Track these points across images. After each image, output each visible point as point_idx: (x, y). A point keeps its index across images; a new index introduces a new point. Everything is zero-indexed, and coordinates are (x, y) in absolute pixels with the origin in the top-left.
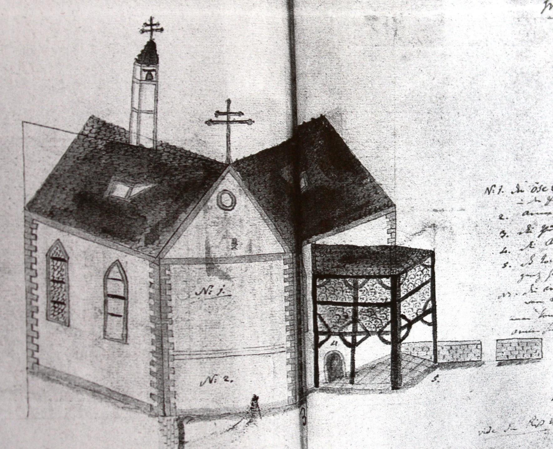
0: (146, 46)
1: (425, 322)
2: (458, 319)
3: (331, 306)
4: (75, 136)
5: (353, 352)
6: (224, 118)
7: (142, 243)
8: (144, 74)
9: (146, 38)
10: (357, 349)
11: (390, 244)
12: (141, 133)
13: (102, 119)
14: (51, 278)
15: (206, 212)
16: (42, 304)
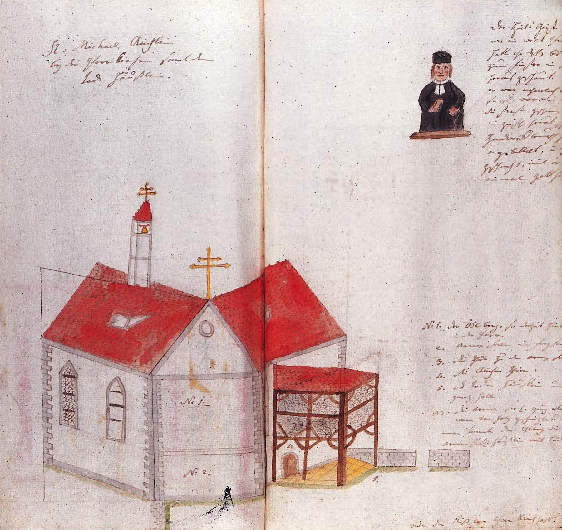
0: (141, 206)
1: (368, 432)
2: (395, 431)
3: (289, 416)
4: (84, 279)
5: (306, 453)
6: (205, 263)
7: (137, 363)
8: (141, 229)
9: (142, 199)
10: (309, 451)
11: (340, 367)
12: (138, 276)
13: (106, 265)
14: (64, 391)
15: (189, 338)
16: (56, 412)
